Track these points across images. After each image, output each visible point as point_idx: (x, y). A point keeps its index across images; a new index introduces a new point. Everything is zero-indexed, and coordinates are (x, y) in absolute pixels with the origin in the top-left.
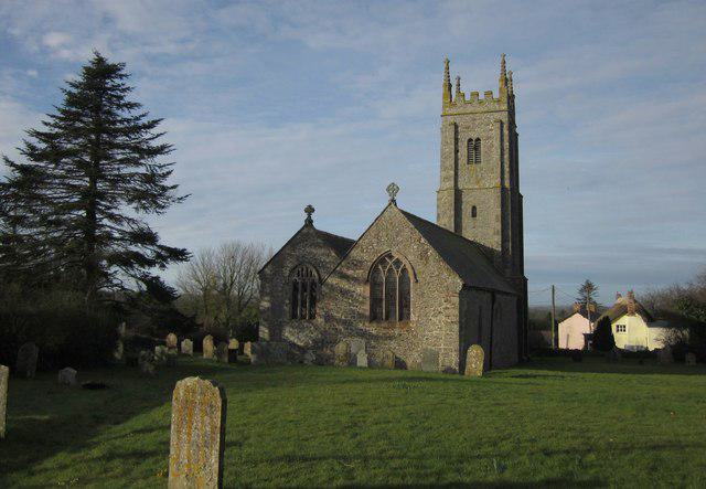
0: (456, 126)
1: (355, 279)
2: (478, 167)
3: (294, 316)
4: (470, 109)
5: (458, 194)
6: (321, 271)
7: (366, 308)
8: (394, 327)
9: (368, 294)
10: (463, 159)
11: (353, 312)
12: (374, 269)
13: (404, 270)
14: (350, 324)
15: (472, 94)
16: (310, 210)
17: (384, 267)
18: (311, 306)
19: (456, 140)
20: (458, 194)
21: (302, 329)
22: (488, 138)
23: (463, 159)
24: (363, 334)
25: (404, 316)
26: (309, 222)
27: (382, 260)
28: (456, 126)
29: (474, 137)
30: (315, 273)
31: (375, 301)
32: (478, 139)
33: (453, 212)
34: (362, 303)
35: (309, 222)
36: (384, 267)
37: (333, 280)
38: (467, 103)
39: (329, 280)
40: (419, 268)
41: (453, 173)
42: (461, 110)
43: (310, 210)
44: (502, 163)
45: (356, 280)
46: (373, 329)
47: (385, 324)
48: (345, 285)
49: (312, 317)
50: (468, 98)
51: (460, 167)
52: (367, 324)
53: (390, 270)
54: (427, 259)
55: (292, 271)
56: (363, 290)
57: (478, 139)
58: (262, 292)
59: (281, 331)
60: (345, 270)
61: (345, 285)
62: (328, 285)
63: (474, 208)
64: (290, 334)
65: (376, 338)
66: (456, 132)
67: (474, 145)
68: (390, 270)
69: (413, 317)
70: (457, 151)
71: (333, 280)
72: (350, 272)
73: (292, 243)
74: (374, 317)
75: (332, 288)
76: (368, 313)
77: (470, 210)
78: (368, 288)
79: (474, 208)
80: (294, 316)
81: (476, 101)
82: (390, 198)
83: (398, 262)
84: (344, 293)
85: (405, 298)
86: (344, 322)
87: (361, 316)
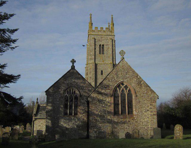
0: (95, 39)
1: (106, 95)
2: (103, 56)
3: (66, 114)
4: (100, 33)
5: (96, 65)
6: (81, 91)
7: (111, 109)
8: (126, 118)
9: (113, 101)
10: (97, 52)
11: (105, 111)
12: (115, 90)
13: (129, 90)
14: (104, 116)
15: (101, 28)
16: (73, 61)
17: (120, 89)
18: (75, 108)
19: (95, 45)
20: (96, 65)
21: (70, 120)
22: (107, 45)
23: (97, 52)
24: (110, 122)
25: (130, 112)
26: (73, 67)
27: (119, 86)
28: (95, 39)
29: (102, 44)
30: (77, 92)
31: (116, 105)
32: (103, 45)
33: (94, 73)
34: (110, 106)
35: (73, 67)
36: (120, 89)
37: (94, 95)
38: (99, 31)
39: (92, 95)
40: (138, 89)
41: (94, 57)
42: (97, 33)
43: (73, 61)
44: (113, 55)
45: (106, 95)
46: (115, 119)
47: (122, 116)
48: (100, 97)
49: (76, 114)
50: (94, 29)
51: (96, 55)
52: (112, 116)
53: (123, 90)
54: (141, 85)
55: (65, 91)
56: (110, 100)
57: (103, 45)
58: (48, 102)
59: (58, 122)
60: (100, 90)
61: (100, 97)
62: (91, 97)
63: (102, 71)
64: (64, 123)
65: (117, 123)
66: (95, 42)
67: (102, 47)
68: (123, 90)
69: (134, 112)
70: (95, 49)
71: (94, 95)
72: (103, 91)
73: (65, 77)
74: (116, 113)
75: (93, 99)
76: (113, 111)
77: (100, 72)
78: (112, 98)
79: (102, 71)
80: (66, 114)
81: (102, 30)
82: (122, 57)
83: (126, 87)
84: (100, 101)
85: (130, 104)
86: (100, 116)
87: (109, 113)
